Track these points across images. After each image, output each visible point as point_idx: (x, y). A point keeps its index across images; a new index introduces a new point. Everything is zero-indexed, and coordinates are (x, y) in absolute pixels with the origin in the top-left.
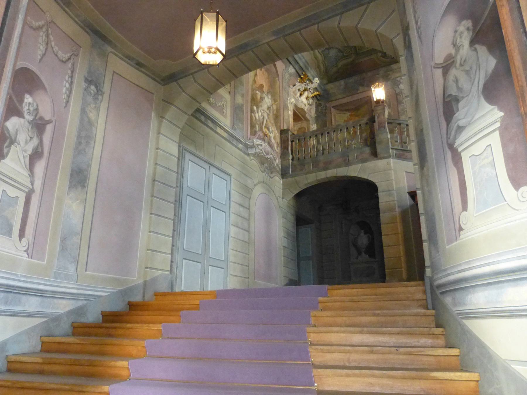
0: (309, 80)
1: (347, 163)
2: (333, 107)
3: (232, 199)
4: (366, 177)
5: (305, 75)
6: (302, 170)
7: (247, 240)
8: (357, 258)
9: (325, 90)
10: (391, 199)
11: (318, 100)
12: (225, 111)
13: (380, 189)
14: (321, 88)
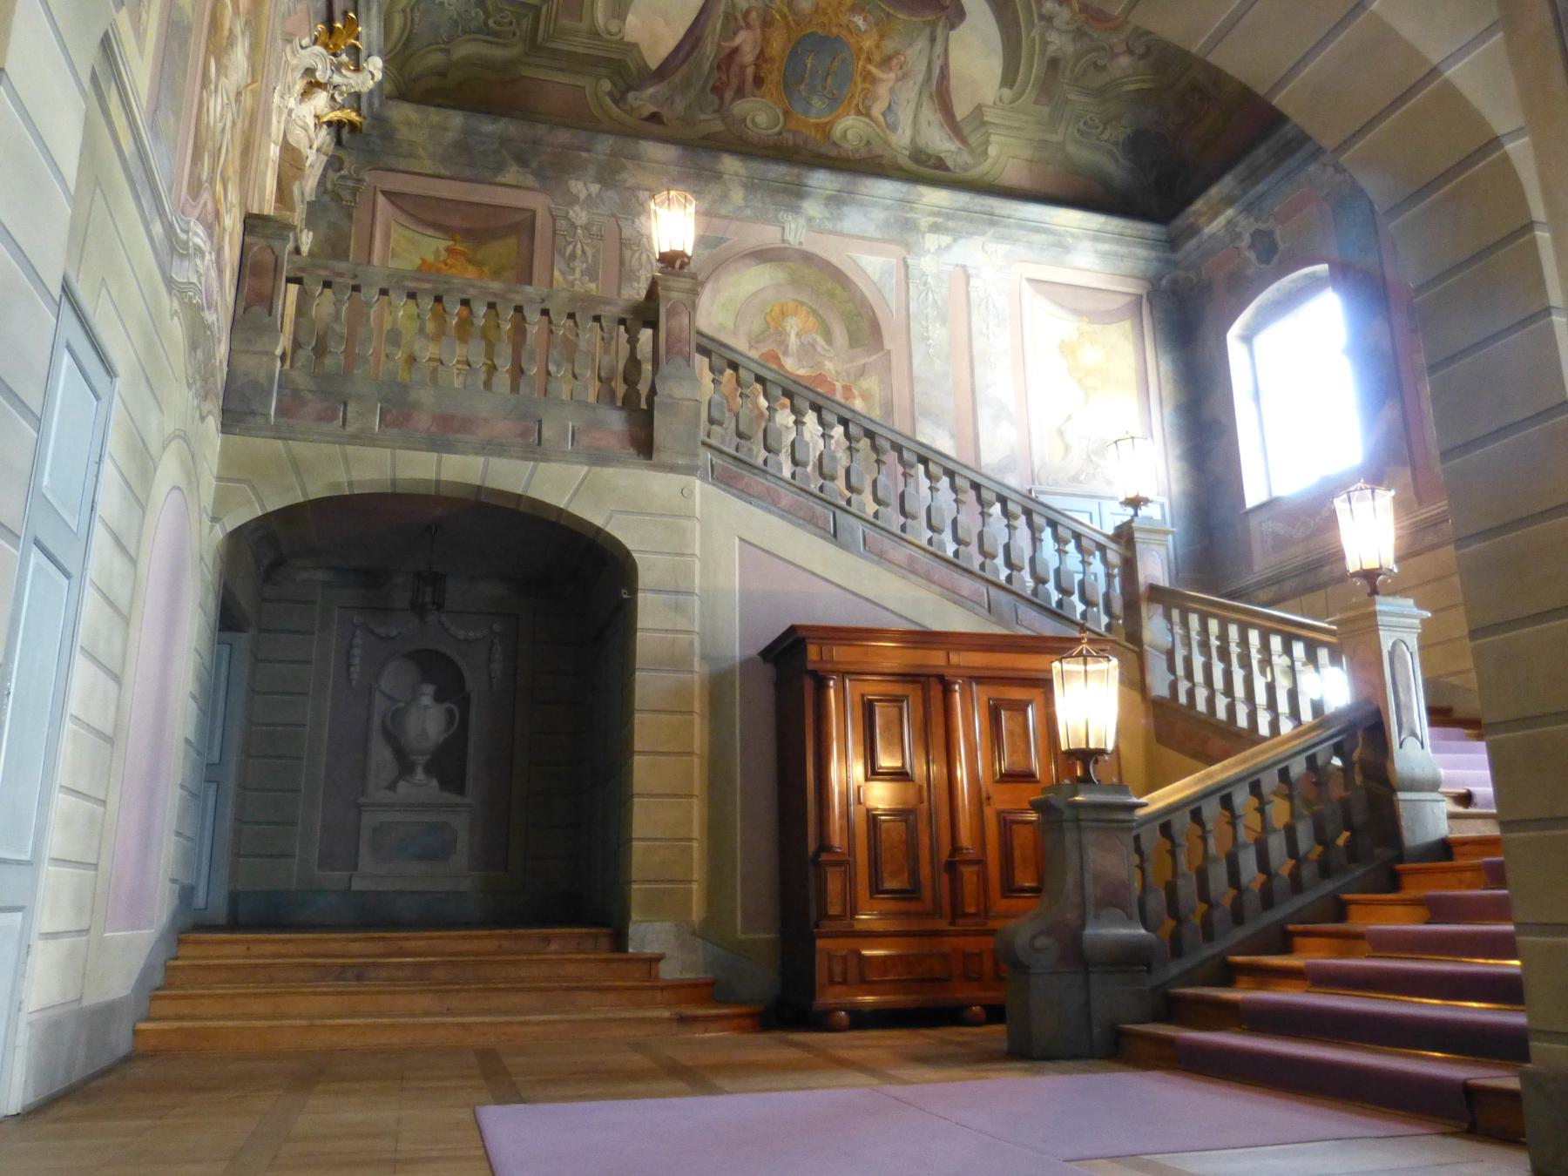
0: (354, 51)
1: (534, 447)
2: (384, 193)
3: (99, 510)
4: (598, 521)
5: (351, 24)
6: (326, 417)
7: (109, 731)
8: (392, 787)
9: (379, 120)
10: (682, 624)
11: (339, 142)
12: (144, 16)
13: (645, 577)
14: (370, 105)
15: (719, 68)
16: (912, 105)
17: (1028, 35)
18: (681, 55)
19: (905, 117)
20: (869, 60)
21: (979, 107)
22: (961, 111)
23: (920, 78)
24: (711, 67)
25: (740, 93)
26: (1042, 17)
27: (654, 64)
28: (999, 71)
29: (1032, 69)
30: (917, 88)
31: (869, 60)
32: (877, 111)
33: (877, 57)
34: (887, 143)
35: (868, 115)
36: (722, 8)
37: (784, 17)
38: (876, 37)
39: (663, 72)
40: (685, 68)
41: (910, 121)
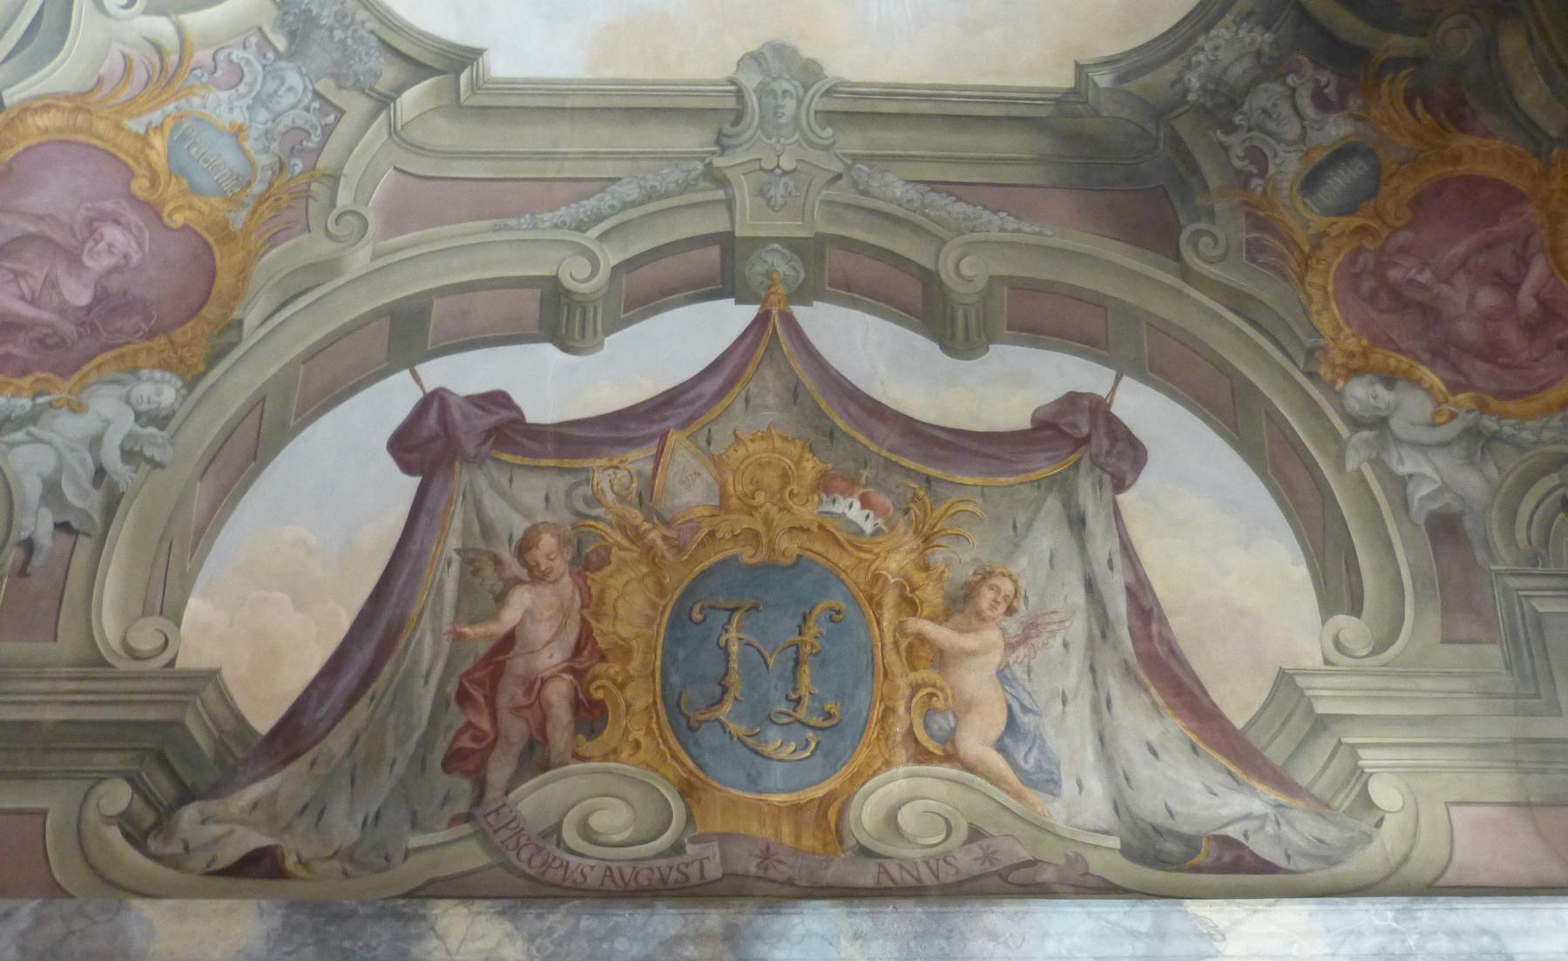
15: (463, 697)
16: (1080, 710)
17: (1340, 467)
18: (348, 678)
19: (1068, 739)
20: (909, 604)
21: (1285, 680)
22: (1239, 700)
23: (1077, 628)
24: (440, 703)
25: (536, 758)
26: (1356, 423)
27: (263, 722)
28: (1300, 573)
29: (1394, 557)
30: (1076, 660)
31: (909, 604)
32: (976, 741)
33: (930, 595)
34: (1041, 827)
35: (951, 757)
36: (454, 542)
37: (636, 536)
38: (910, 542)
39: (292, 735)
40: (361, 711)
41: (1090, 754)
